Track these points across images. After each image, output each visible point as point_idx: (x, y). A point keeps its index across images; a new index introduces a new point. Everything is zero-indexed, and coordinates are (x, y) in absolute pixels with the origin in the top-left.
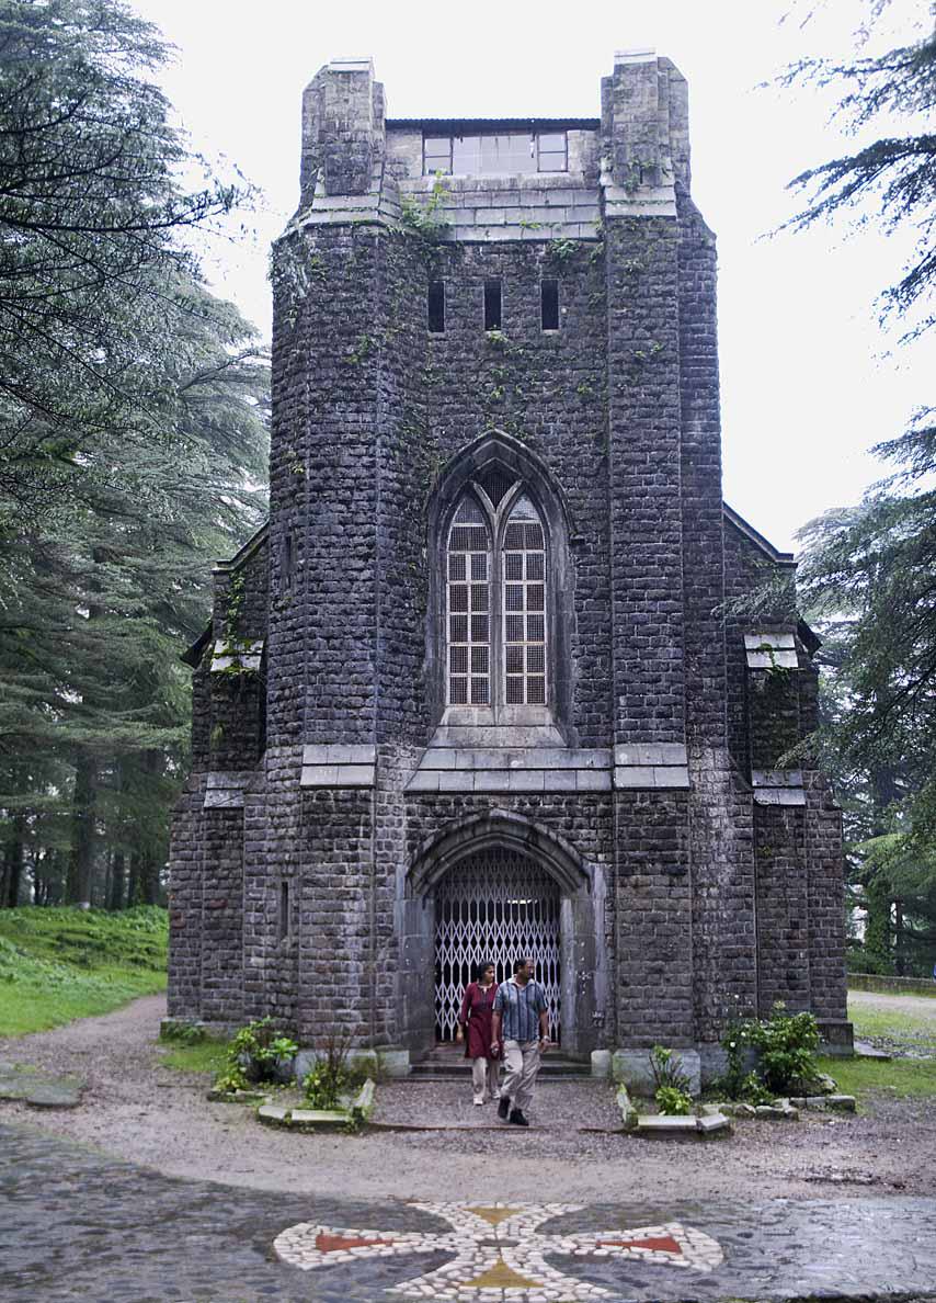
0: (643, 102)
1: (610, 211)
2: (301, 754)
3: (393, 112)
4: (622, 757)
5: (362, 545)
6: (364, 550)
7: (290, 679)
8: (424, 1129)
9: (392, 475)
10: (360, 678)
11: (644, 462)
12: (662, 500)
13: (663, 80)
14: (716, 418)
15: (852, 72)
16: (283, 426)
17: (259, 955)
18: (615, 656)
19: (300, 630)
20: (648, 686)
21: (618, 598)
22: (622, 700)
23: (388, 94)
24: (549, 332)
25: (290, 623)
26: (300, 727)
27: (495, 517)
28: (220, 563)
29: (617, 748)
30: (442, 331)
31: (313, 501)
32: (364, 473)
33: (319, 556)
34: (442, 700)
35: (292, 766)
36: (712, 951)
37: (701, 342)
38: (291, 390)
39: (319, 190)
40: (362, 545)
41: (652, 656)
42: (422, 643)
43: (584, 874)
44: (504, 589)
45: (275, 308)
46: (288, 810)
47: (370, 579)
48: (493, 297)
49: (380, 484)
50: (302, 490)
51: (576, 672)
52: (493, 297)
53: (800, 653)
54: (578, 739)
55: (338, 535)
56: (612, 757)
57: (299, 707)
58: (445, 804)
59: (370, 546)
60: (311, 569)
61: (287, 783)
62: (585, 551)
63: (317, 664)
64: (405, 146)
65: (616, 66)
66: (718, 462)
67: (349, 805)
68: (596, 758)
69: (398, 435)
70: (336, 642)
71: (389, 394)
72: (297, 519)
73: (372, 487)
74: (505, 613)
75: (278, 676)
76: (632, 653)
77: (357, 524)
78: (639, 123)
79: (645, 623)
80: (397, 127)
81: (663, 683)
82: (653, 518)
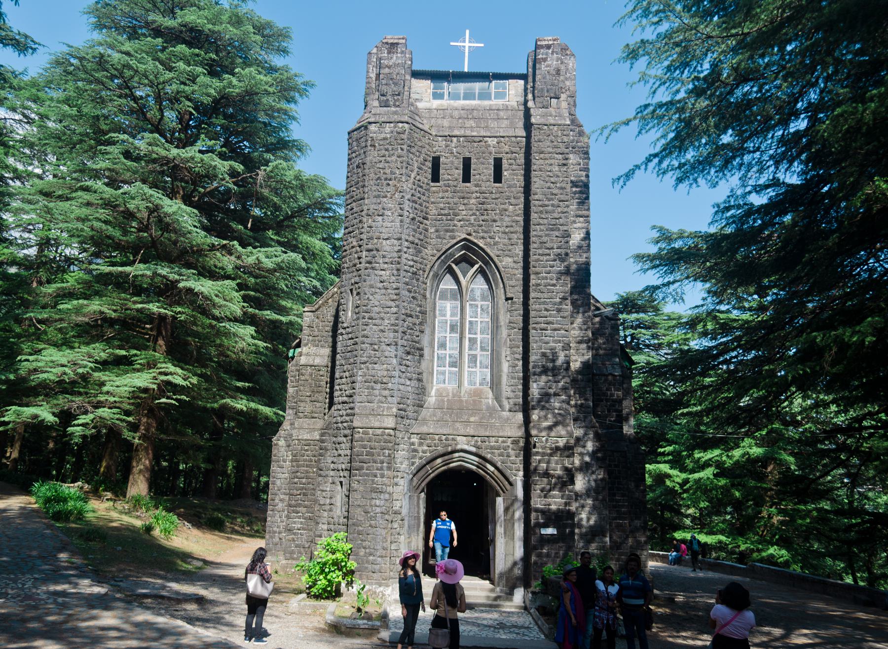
8: (337, 316)
9: (410, 257)
11: (549, 255)
15: (640, 132)
24: (497, 185)
25: (350, 336)
32: (395, 255)
42: (422, 349)
43: (511, 484)
46: (408, 383)
49: (404, 261)
54: (507, 407)
61: (345, 424)
69: (414, 236)
73: (399, 263)
74: (467, 336)
75: (342, 365)
82: (554, 285)
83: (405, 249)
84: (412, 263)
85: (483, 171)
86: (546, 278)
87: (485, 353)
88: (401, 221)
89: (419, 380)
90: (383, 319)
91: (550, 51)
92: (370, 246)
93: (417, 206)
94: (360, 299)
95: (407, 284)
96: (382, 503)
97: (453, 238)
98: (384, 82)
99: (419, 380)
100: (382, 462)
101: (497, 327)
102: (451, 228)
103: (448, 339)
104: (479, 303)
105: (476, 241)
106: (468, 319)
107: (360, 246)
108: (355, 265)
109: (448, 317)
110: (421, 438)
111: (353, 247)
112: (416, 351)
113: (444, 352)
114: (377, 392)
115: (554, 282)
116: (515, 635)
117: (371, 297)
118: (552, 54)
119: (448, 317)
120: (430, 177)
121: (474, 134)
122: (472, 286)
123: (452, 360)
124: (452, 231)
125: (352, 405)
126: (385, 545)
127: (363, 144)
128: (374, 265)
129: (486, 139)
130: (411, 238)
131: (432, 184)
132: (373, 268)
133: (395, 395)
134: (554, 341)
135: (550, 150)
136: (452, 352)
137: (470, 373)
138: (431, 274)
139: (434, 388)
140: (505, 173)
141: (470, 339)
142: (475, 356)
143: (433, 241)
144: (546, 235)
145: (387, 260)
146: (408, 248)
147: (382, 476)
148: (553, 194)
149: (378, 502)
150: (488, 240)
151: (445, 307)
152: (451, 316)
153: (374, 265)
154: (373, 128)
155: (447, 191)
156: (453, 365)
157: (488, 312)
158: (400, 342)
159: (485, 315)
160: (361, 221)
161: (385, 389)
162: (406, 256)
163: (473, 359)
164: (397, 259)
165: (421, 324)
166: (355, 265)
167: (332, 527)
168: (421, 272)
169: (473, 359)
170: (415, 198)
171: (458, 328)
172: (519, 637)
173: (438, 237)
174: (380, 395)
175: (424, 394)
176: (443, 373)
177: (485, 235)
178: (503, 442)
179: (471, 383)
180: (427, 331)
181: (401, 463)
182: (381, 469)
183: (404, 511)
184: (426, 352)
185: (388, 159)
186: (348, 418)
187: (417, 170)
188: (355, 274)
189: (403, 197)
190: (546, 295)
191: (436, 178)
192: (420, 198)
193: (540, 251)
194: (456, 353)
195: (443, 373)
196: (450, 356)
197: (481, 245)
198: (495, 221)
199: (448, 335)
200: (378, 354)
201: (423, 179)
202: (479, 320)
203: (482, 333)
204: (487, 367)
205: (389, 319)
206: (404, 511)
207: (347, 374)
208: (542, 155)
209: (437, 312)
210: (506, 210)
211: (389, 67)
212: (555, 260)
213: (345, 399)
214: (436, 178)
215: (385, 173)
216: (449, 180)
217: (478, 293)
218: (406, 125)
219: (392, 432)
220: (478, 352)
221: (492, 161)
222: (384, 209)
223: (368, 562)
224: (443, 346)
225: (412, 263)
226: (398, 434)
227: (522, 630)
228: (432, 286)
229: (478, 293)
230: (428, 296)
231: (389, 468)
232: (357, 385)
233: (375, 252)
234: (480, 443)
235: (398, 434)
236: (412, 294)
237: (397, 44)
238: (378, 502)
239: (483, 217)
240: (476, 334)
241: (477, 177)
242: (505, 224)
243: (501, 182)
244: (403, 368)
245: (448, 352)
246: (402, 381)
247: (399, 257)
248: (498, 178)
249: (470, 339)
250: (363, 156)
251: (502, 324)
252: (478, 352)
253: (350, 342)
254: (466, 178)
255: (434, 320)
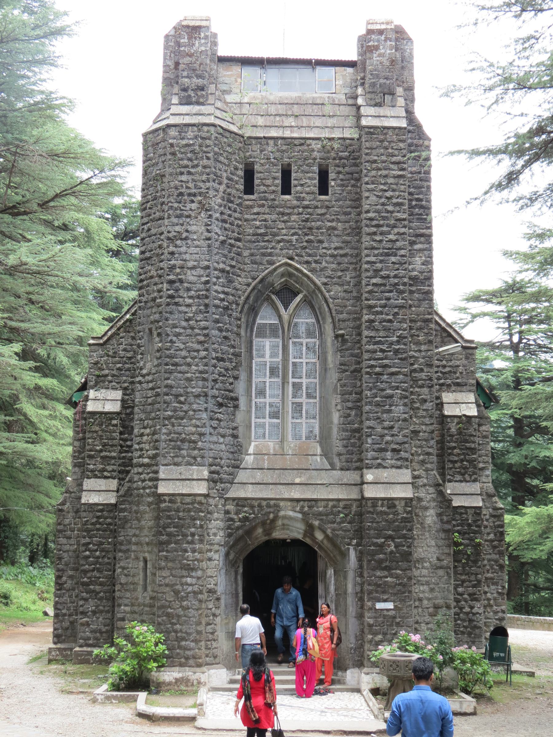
0: (387, 50)
1: (364, 122)
2: (157, 472)
3: (222, 52)
4: (369, 477)
5: (199, 334)
6: (202, 338)
7: (150, 422)
9: (220, 289)
10: (198, 423)
12: (396, 310)
13: (400, 36)
14: (431, 257)
16: (148, 254)
17: (126, 605)
18: (364, 411)
19: (159, 390)
20: (386, 432)
21: (367, 373)
22: (369, 440)
23: (220, 40)
24: (323, 197)
25: (151, 385)
26: (157, 454)
27: (285, 315)
28: (93, 338)
29: (365, 471)
30: (253, 194)
31: (168, 304)
32: (202, 286)
33: (171, 341)
34: (250, 438)
35: (151, 480)
36: (425, 602)
37: (422, 207)
38: (153, 231)
39: (175, 100)
40: (199, 334)
41: (389, 411)
42: (237, 399)
44: (290, 385)
45: (143, 177)
46: (221, 440)
47: (205, 358)
48: (286, 174)
50: (161, 297)
51: (336, 418)
52: (286, 174)
53: (478, 406)
54: (338, 465)
55: (184, 328)
56: (362, 476)
57: (157, 441)
58: (252, 507)
59: (206, 335)
60: (167, 349)
61: (148, 491)
62: (344, 341)
63: (169, 413)
64: (228, 74)
65: (136, 701)
66: (431, 285)
67: (190, 506)
68: (352, 476)
69: (224, 263)
70: (182, 399)
71: (219, 235)
72: (157, 316)
74: (291, 380)
76: (376, 410)
77: (197, 321)
78: (382, 66)
79: (385, 390)
80: (223, 60)
81: (395, 431)
82: (390, 321)
83: (215, 280)
84: (222, 296)
85: (305, 181)
86: (381, 313)
87: (312, 401)
88: (209, 246)
89: (235, 436)
90: (189, 365)
91: (383, 38)
92: (172, 277)
93: (227, 226)
94: (161, 341)
95: (217, 321)
96: (194, 581)
97: (271, 263)
98: (185, 74)
99: (235, 436)
100: (193, 535)
101: (326, 370)
102: (269, 251)
103: (267, 384)
104: (304, 341)
105: (298, 266)
106: (292, 360)
107: (160, 277)
108: (154, 300)
109: (267, 358)
110: (237, 505)
111: (152, 277)
112: (230, 402)
113: (262, 400)
114: (184, 452)
115: (391, 317)
116: (343, 717)
117: (174, 339)
118: (385, 40)
119: (267, 358)
120: (242, 187)
121: (295, 135)
122: (295, 320)
123: (272, 409)
124: (270, 254)
125: (155, 468)
126: (199, 628)
127: (161, 151)
128: (177, 300)
129: (308, 142)
130: (221, 266)
131: (246, 197)
132: (176, 304)
133: (206, 455)
134: (392, 388)
135: (384, 158)
136: (272, 400)
137: (295, 425)
138: (246, 306)
139: (253, 444)
140: (333, 183)
141: (294, 384)
142: (300, 405)
143: (248, 268)
144: (381, 262)
145: (192, 293)
146: (218, 278)
147: (194, 551)
148: (388, 212)
149: (189, 580)
150: (314, 265)
151: (264, 346)
152: (271, 357)
153: (177, 300)
154: (173, 132)
155: (263, 206)
156: (274, 415)
157: (314, 352)
158: (211, 393)
159: (312, 355)
160: (160, 247)
161: (194, 449)
162: (216, 287)
163: (298, 407)
164: (204, 293)
165: (235, 368)
166: (154, 300)
167: (136, 608)
168: (234, 306)
169: (298, 407)
170: (226, 217)
171: (279, 371)
172: (347, 719)
173: (254, 262)
174: (188, 456)
175: (240, 452)
176: (263, 426)
177: (310, 259)
178: (334, 506)
179: (297, 437)
180: (243, 376)
181: (215, 535)
182: (192, 542)
183: (220, 589)
184: (242, 402)
185: (192, 170)
186: (150, 484)
187: (226, 181)
188: (154, 310)
189: (210, 216)
190: (382, 334)
191: (249, 188)
192: (230, 216)
193: (374, 281)
194: (277, 400)
195: (263, 426)
196: (271, 405)
197: (305, 271)
198: (321, 242)
199: (268, 380)
200: (185, 407)
201: (234, 192)
202: (304, 361)
203: (308, 376)
204: (314, 418)
205: (197, 365)
206: (220, 589)
207: (148, 431)
208: (374, 166)
209: (254, 352)
210: (334, 228)
211: (191, 55)
212: (391, 291)
213: (146, 460)
214: (249, 188)
215: (187, 188)
216: (266, 192)
217: (302, 329)
218: (212, 129)
219: (202, 499)
220: (303, 400)
221: (316, 169)
222: (187, 231)
223: (180, 647)
224: (261, 393)
225: (222, 296)
226: (211, 501)
227: (351, 713)
228: (247, 321)
229: (302, 329)
230: (243, 333)
231: (201, 541)
232: (162, 445)
233: (178, 284)
234: (306, 509)
235: (211, 501)
236: (224, 334)
237: (199, 27)
238: (189, 580)
239: (307, 238)
240: (301, 378)
241: (299, 188)
242: (333, 246)
243: (327, 194)
244: (215, 423)
245: (268, 400)
246: (214, 439)
247: (207, 290)
248: (323, 189)
249: (294, 384)
250: (160, 165)
251: (331, 366)
252: (303, 400)
253: (150, 393)
254: (286, 189)
255: (251, 363)
